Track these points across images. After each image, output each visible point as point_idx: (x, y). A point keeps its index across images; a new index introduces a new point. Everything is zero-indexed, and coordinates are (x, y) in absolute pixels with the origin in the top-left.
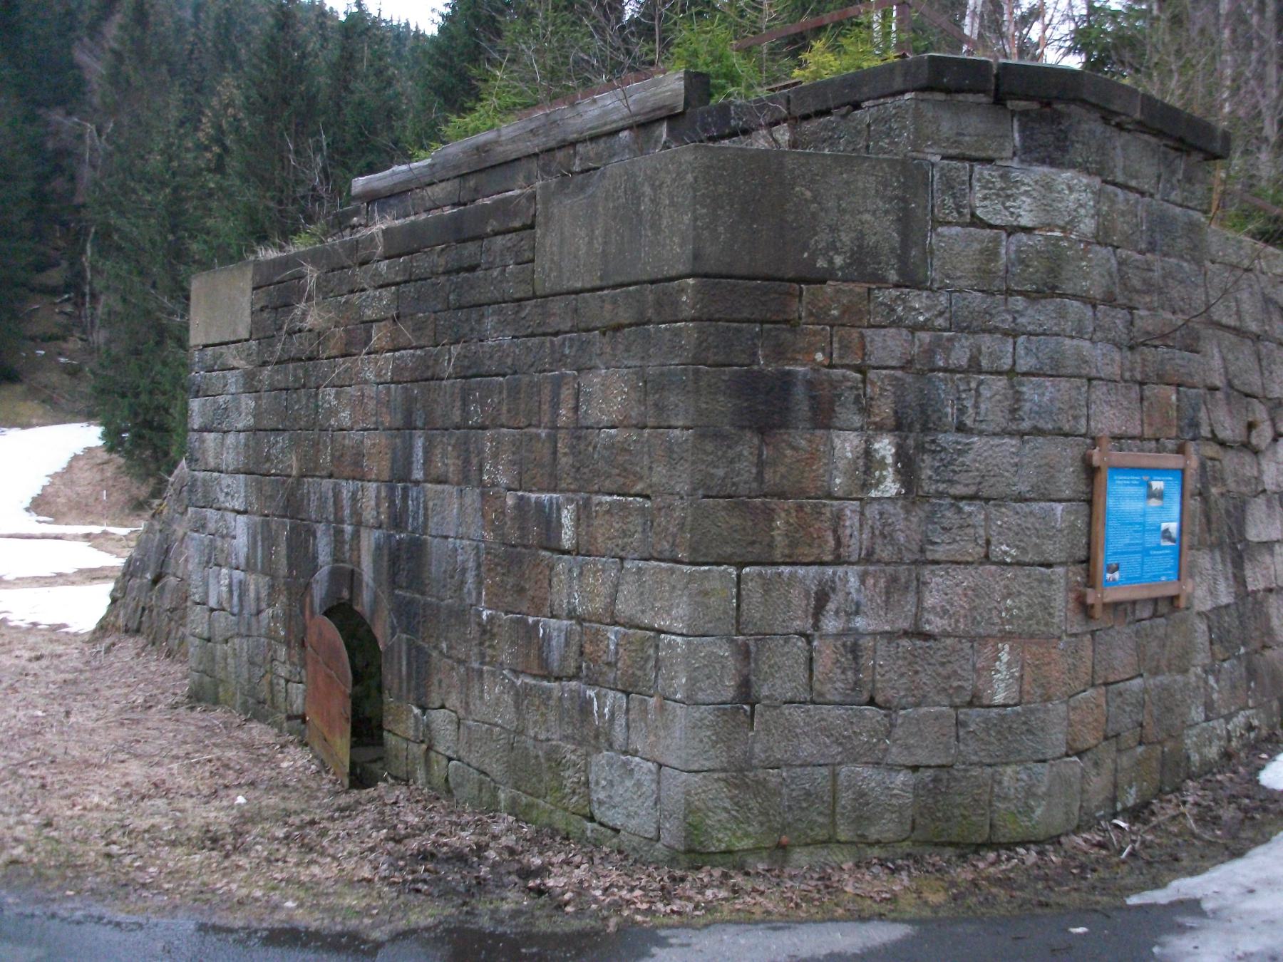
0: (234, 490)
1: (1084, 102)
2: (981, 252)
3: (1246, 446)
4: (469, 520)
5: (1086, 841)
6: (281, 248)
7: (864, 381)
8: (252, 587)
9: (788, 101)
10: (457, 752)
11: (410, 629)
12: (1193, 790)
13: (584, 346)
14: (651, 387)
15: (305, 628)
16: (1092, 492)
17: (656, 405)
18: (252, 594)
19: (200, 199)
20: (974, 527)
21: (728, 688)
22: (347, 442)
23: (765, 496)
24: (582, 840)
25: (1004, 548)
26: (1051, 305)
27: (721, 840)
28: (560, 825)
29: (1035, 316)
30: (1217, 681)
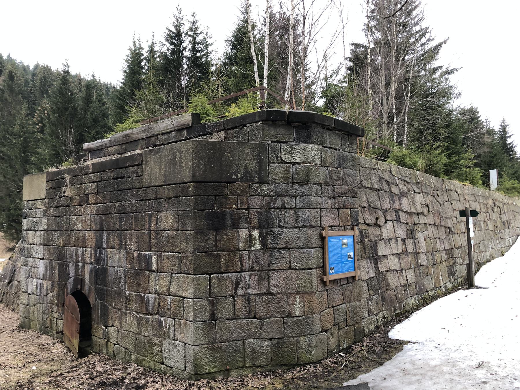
0: (39, 251)
1: (316, 123)
2: (284, 171)
3: (376, 225)
4: (122, 261)
5: (330, 361)
6: (57, 168)
7: (248, 213)
8: (45, 285)
9: (224, 124)
10: (117, 342)
11: (102, 299)
12: (366, 341)
13: (159, 204)
14: (179, 217)
15: (64, 299)
16: (323, 245)
17: (182, 223)
18: (45, 288)
19: (34, 141)
20: (285, 258)
21: (207, 315)
22: (80, 234)
23: (218, 251)
24: (160, 372)
25: (295, 264)
26: (307, 187)
27: (207, 369)
28: (153, 367)
29: (301, 190)
30: (372, 303)
